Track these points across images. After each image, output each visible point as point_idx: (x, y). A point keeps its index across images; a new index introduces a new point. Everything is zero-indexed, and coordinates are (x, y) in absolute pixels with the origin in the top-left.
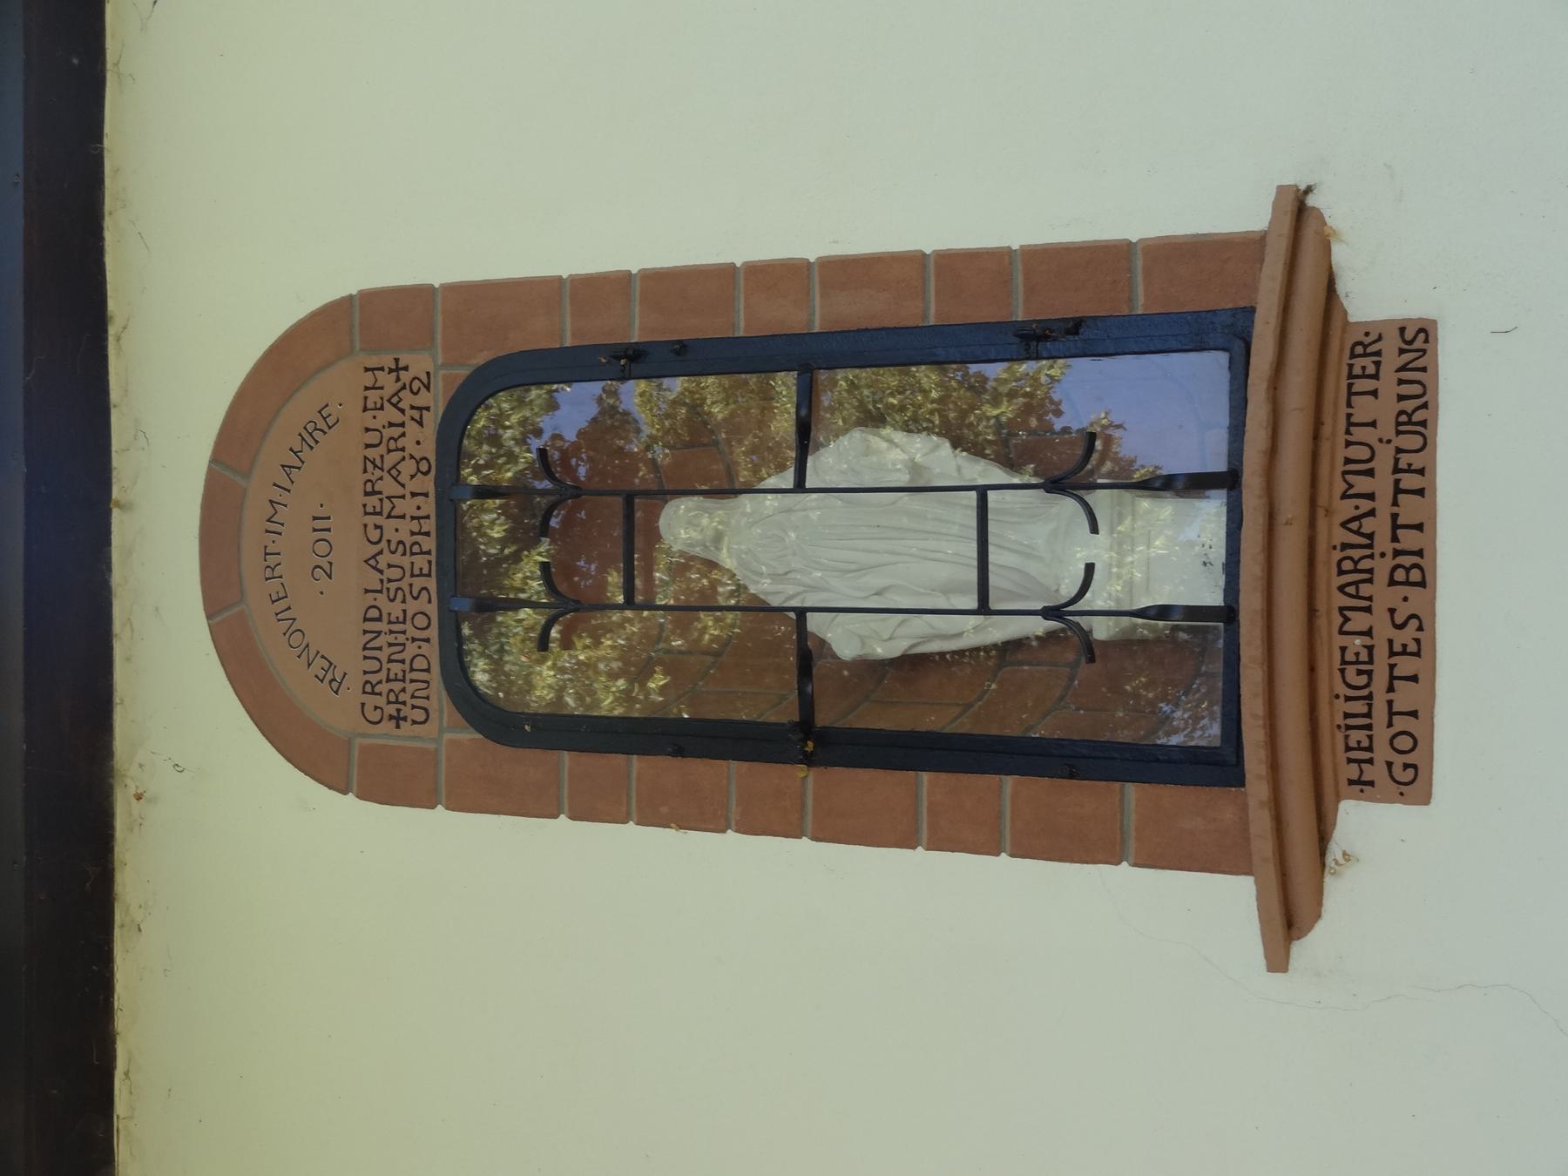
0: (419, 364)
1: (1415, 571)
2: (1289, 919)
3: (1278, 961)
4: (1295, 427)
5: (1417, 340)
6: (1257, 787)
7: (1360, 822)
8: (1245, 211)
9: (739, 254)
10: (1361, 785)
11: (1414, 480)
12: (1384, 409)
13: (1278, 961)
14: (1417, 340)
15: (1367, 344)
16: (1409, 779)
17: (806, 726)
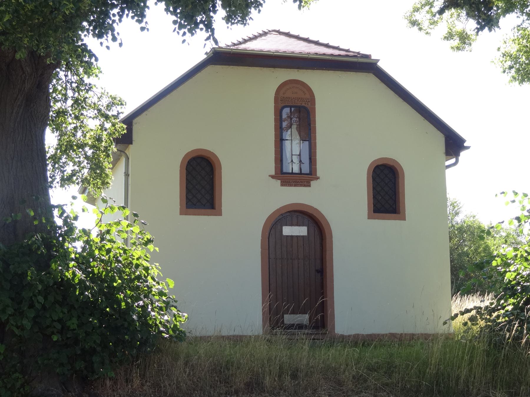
0: (309, 104)
1: (295, 186)
2: (272, 177)
3: (269, 176)
4: (289, 178)
5: (309, 186)
6: (281, 175)
7: (279, 181)
8: (318, 174)
9: (317, 135)
10: (281, 182)
11: (301, 186)
12: (305, 184)
13: (269, 176)
14: (309, 186)
15: (309, 183)
16: (282, 185)
17: (283, 140)
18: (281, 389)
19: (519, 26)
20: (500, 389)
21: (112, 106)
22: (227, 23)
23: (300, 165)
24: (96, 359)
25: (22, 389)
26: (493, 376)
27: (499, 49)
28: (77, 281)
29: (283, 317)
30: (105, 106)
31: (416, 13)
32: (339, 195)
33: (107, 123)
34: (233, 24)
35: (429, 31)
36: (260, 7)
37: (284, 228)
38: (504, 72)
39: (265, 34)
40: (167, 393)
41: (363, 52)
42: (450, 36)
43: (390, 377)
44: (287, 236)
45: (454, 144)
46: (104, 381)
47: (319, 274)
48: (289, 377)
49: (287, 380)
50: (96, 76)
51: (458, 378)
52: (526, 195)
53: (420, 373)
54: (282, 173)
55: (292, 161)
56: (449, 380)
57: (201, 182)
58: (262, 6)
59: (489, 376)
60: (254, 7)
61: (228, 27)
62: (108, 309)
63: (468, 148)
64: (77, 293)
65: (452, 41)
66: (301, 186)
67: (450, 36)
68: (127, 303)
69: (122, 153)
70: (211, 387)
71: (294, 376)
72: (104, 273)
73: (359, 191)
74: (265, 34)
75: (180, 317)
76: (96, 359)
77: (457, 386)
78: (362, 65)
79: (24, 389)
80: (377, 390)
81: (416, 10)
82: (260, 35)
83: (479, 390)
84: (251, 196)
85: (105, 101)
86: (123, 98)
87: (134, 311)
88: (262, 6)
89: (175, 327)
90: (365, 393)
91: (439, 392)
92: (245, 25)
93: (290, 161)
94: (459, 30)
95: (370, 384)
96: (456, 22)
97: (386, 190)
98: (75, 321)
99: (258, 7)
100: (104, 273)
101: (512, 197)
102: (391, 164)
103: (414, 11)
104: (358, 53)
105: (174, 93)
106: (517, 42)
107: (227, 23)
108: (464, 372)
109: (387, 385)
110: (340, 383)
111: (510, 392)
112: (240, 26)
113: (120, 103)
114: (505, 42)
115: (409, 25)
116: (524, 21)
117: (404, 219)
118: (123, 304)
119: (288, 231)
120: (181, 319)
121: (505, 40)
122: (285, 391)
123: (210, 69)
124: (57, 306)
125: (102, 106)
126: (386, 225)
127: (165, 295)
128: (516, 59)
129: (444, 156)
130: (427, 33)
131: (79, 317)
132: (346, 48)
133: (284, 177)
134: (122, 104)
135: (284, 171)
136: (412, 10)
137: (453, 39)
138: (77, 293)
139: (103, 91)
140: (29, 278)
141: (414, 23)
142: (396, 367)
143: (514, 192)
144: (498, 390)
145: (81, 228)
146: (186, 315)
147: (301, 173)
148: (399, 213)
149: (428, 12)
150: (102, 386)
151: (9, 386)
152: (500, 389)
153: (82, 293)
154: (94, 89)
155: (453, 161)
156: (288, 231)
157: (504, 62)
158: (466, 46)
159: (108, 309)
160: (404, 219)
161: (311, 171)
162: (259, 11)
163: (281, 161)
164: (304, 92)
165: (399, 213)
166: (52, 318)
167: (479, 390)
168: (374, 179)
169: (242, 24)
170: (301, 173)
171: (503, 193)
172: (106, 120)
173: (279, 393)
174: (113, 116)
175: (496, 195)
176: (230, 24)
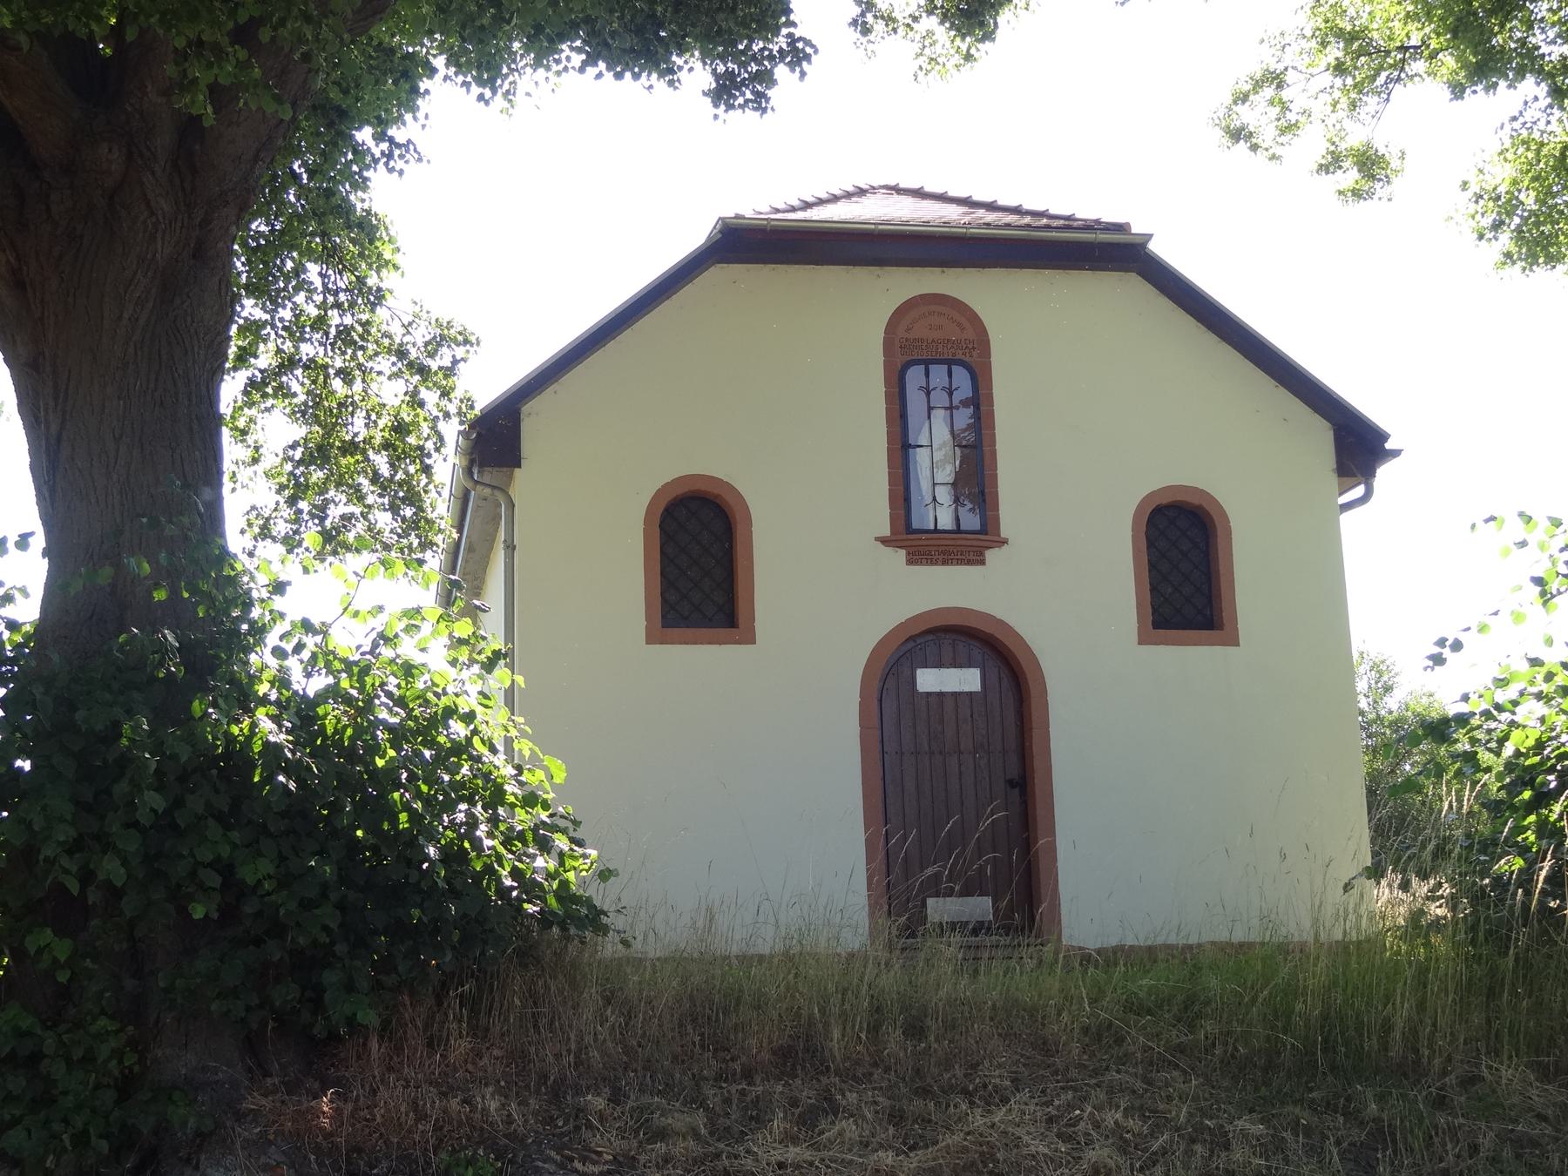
1: (945, 563)
2: (884, 541)
3: (877, 539)
5: (983, 563)
13: (877, 539)
14: (983, 563)
15: (982, 554)
16: (910, 562)
18: (875, 1065)
19: (1514, 119)
20: (1510, 1057)
21: (439, 345)
22: (716, 106)
23: (956, 510)
24: (330, 977)
25: (114, 1062)
26: (1488, 1021)
27: (1465, 185)
28: (257, 747)
29: (924, 905)
30: (420, 343)
31: (1239, 108)
32: (1063, 584)
33: (428, 388)
34: (730, 107)
35: (1278, 151)
36: (805, 64)
37: (919, 672)
38: (1481, 237)
39: (861, 192)
40: (546, 1077)
41: (1109, 217)
42: (1332, 163)
43: (1192, 1028)
44: (929, 694)
45: (1358, 448)
46: (365, 1044)
47: (1016, 791)
48: (899, 1032)
49: (894, 1040)
50: (396, 267)
51: (1387, 1027)
52: (1557, 523)
53: (1277, 1018)
54: (909, 529)
55: (934, 499)
56: (1361, 1035)
57: (699, 562)
58: (809, 62)
59: (1477, 1019)
60: (789, 64)
61: (716, 117)
62: (359, 833)
63: (1396, 453)
64: (256, 779)
65: (1339, 172)
66: (960, 562)
67: (1332, 163)
68: (414, 817)
69: (497, 493)
70: (675, 1058)
71: (915, 1030)
72: (349, 732)
73: (1115, 575)
74: (861, 192)
75: (575, 858)
76: (330, 977)
77: (1386, 1050)
78: (1110, 252)
79: (121, 1062)
80: (1151, 1064)
81: (1242, 98)
82: (848, 195)
83: (1449, 1059)
84: (832, 591)
85: (421, 335)
86: (470, 329)
87: (433, 838)
88: (809, 62)
89: (564, 890)
90: (1118, 1072)
91: (1333, 1068)
92: (764, 110)
93: (929, 499)
94: (1356, 145)
95: (1132, 1049)
96: (1347, 124)
97: (1184, 568)
98: (266, 867)
99: (799, 62)
100: (349, 732)
101: (1517, 530)
102: (1195, 500)
103: (1235, 102)
104: (1098, 222)
105: (627, 336)
106: (1510, 156)
107: (716, 106)
108: (1403, 1011)
109: (1181, 1049)
110: (1046, 1047)
111: (1539, 1064)
112: (751, 115)
113: (460, 338)
114: (1481, 171)
115: (1226, 140)
116: (1526, 103)
117: (1234, 641)
118: (403, 817)
119: (929, 680)
120: (576, 864)
121: (1481, 166)
122: (887, 1070)
123: (718, 274)
124: (211, 822)
125: (414, 345)
126: (1188, 661)
127: (546, 805)
128: (1510, 206)
129: (1333, 479)
130: (1273, 157)
131: (282, 859)
132: (1068, 213)
133: (915, 542)
134: (466, 342)
135: (915, 525)
136: (1229, 100)
137: (1340, 167)
138: (256, 779)
139: (417, 309)
140: (124, 741)
141: (1237, 134)
142: (1208, 1003)
143: (1521, 514)
144: (1505, 1057)
145: (298, 618)
146: (594, 853)
147: (958, 531)
148: (1221, 627)
149: (1271, 103)
150: (359, 1057)
151: (78, 1053)
152: (1510, 1057)
153: (269, 779)
154: (389, 301)
155: (1359, 491)
156: (929, 680)
157: (1478, 217)
158: (1378, 185)
159: (359, 833)
160: (1234, 641)
161: (984, 524)
162: (803, 74)
163: (907, 500)
164: (959, 325)
165: (1221, 627)
166: (194, 856)
167: (1449, 1059)
168: (1151, 544)
169: (755, 109)
170: (958, 531)
171: (1493, 519)
172: (425, 380)
173: (871, 1074)
174: (441, 368)
175: (1473, 526)
176: (723, 107)
